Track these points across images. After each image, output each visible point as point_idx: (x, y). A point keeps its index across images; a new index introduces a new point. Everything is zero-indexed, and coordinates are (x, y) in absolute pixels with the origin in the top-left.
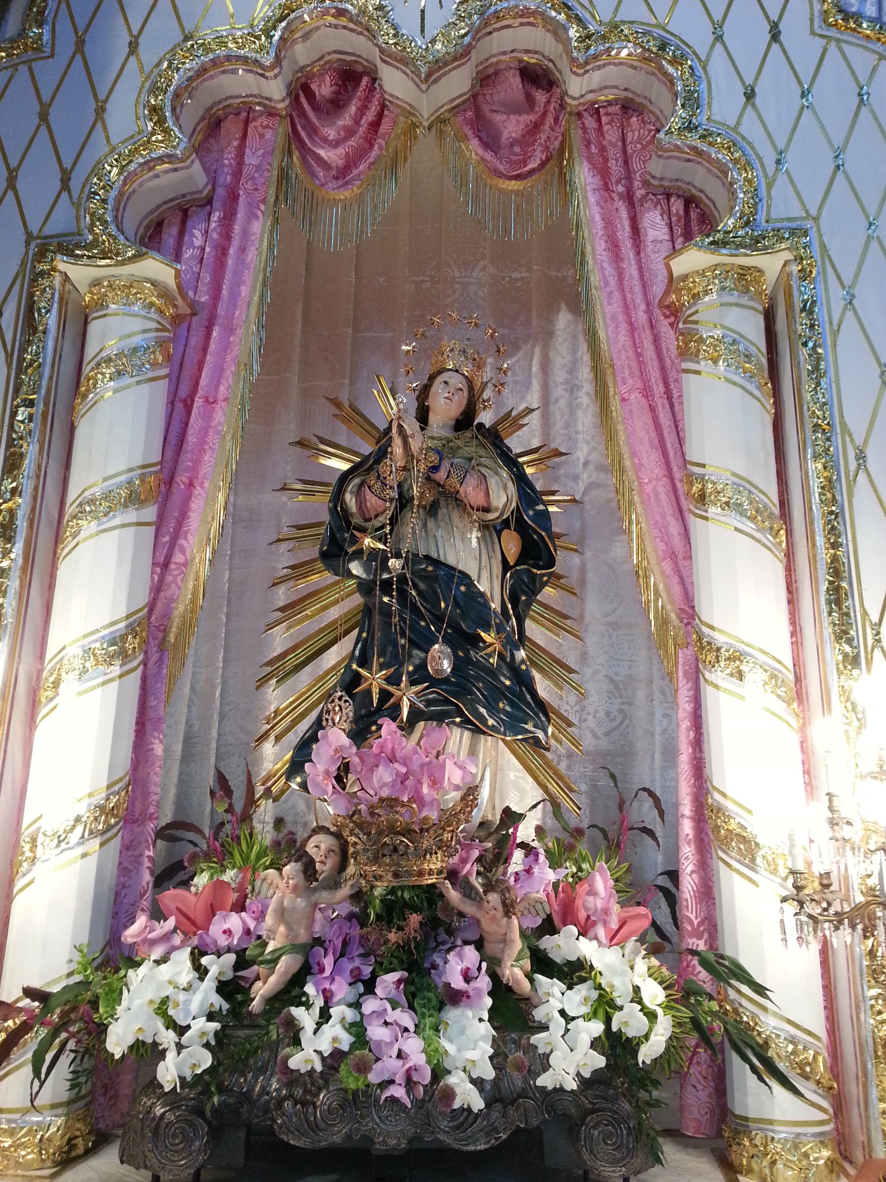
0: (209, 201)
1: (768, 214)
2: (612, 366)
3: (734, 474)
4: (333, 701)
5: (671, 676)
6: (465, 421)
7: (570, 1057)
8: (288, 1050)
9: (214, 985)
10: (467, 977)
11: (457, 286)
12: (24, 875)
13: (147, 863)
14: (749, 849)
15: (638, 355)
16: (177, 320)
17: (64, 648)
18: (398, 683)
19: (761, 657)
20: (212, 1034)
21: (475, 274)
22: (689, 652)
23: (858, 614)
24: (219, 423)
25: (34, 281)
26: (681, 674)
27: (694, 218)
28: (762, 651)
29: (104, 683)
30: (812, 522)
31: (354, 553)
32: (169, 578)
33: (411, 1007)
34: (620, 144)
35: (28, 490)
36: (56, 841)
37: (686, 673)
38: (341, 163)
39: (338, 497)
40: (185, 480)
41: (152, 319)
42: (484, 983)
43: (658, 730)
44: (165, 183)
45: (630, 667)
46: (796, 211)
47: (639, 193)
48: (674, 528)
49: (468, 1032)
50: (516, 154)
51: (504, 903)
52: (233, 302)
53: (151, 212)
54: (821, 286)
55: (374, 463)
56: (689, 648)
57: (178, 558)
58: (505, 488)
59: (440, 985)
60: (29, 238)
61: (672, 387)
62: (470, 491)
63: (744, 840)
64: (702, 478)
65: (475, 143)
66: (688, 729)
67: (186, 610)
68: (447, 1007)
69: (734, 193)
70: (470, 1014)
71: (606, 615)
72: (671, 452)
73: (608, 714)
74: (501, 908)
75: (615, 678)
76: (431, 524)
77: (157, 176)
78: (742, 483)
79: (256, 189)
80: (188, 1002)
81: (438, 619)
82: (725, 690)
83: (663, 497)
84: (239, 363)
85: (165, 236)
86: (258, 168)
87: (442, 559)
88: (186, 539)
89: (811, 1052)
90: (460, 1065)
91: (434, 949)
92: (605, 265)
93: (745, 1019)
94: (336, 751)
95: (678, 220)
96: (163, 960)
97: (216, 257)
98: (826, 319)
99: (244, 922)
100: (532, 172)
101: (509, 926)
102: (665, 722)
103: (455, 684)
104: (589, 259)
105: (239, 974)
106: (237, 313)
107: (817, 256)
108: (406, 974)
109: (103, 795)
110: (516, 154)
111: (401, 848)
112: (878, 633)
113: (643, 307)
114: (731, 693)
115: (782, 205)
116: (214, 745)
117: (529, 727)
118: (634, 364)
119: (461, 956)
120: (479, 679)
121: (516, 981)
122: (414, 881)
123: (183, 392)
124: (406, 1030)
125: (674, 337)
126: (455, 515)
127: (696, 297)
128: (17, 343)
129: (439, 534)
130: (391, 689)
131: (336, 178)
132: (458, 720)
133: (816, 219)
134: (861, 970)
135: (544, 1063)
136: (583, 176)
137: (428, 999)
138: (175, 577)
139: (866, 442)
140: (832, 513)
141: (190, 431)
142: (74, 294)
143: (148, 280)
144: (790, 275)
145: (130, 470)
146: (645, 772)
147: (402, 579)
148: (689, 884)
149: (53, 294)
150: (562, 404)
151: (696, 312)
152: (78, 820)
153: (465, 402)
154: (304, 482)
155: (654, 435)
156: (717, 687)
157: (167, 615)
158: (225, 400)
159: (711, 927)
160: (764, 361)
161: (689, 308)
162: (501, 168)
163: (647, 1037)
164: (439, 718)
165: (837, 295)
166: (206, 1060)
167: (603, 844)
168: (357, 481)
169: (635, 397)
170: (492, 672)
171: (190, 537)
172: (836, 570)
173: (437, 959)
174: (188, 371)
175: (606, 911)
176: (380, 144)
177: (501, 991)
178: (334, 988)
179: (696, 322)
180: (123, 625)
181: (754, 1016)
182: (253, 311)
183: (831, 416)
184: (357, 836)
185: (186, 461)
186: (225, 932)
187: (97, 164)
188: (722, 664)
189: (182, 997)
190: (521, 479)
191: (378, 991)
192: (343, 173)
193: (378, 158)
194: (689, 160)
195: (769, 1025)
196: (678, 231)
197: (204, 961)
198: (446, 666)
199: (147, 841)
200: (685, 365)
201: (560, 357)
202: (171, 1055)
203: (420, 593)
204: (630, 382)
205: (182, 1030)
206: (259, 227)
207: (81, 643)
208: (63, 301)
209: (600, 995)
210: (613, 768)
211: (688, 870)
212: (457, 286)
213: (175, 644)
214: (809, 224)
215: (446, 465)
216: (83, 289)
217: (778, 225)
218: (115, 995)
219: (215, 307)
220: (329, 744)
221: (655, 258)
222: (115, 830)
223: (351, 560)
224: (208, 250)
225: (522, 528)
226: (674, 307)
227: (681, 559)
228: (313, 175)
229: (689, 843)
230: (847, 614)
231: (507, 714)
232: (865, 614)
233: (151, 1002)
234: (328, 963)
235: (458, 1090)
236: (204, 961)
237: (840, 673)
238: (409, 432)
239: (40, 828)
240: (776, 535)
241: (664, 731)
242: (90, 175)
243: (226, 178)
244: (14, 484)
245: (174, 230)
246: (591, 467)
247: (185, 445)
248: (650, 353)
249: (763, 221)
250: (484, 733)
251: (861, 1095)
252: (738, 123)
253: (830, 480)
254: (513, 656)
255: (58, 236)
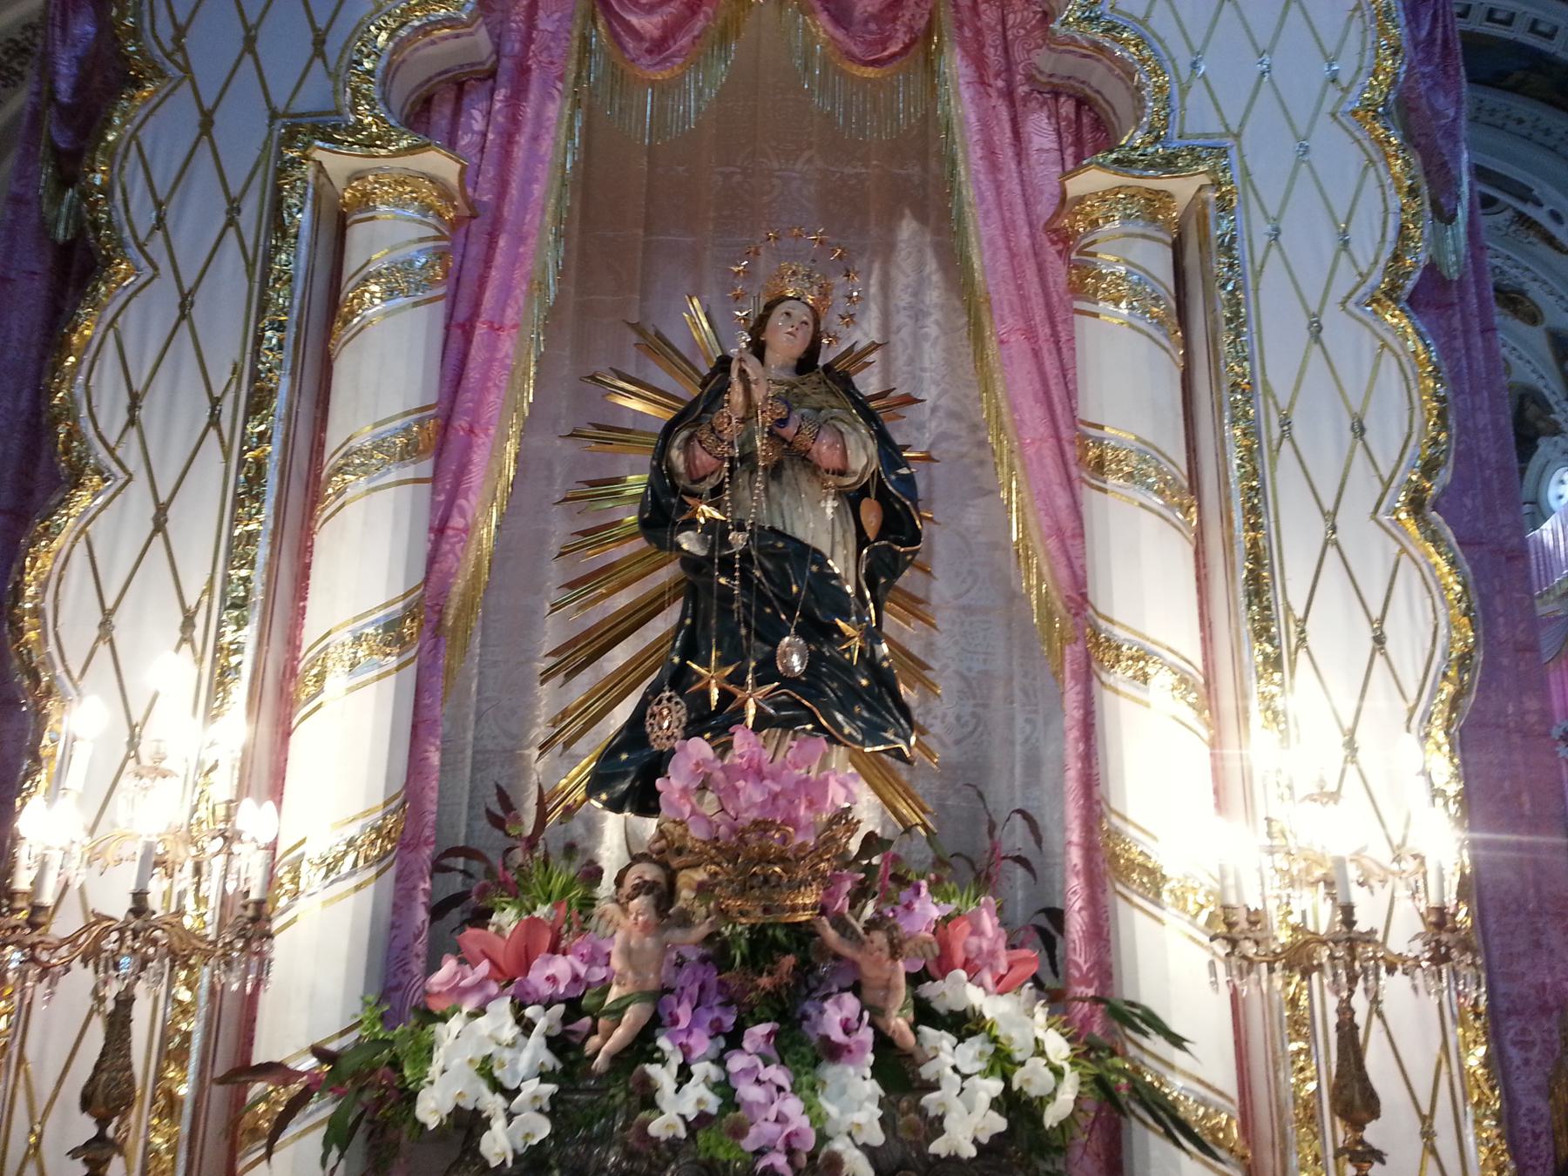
0: (492, 74)
1: (1182, 128)
2: (988, 301)
3: (1138, 439)
4: (660, 702)
5: (1057, 675)
6: (806, 363)
7: (967, 1119)
8: (643, 1115)
9: (543, 1041)
10: (847, 1030)
11: (776, 181)
12: (282, 913)
13: (422, 898)
14: (1154, 880)
15: (1019, 287)
16: (454, 225)
17: (329, 633)
18: (742, 683)
19: (1170, 657)
20: (546, 1099)
21: (798, 166)
22: (1079, 648)
23: (1281, 609)
24: (507, 356)
25: (281, 172)
26: (1068, 674)
27: (1090, 128)
28: (1169, 650)
29: (379, 677)
30: (1228, 499)
31: (684, 522)
32: (446, 547)
33: (782, 1063)
34: (999, 28)
35: (278, 438)
36: (324, 870)
37: (1074, 672)
38: (657, 33)
39: (662, 453)
40: (464, 424)
41: (428, 224)
42: (866, 1035)
43: (1019, 738)
44: (445, 51)
45: (985, 661)
46: (1214, 126)
47: (1022, 90)
48: (1062, 500)
49: (851, 1091)
50: (871, 33)
51: (891, 942)
52: (524, 205)
53: (421, 86)
54: (1240, 216)
55: (705, 410)
56: (1083, 644)
57: (457, 522)
58: (865, 448)
59: (815, 1040)
60: (274, 115)
61: (1060, 328)
62: (824, 451)
63: (1151, 872)
64: (1099, 442)
65: (823, 19)
66: (1077, 740)
67: (467, 586)
68: (824, 1063)
69: (1141, 100)
70: (851, 1070)
71: (958, 597)
72: (1059, 409)
73: (958, 718)
74: (887, 949)
75: (966, 673)
76: (773, 489)
77: (433, 43)
78: (1148, 452)
79: (552, 63)
80: (515, 1061)
81: (790, 606)
82: (1127, 696)
83: (1049, 461)
84: (532, 281)
85: (435, 117)
86: (554, 35)
87: (789, 532)
88: (466, 499)
89: (1224, 1116)
90: (844, 1128)
91: (808, 996)
92: (982, 177)
93: (1149, 1079)
94: (697, 765)
95: (1069, 126)
96: (480, 1011)
97: (502, 147)
98: (1248, 257)
99: (572, 966)
100: (893, 56)
101: (894, 971)
102: (1028, 729)
103: (807, 684)
104: (961, 169)
105: (570, 1027)
106: (528, 217)
107: (1238, 181)
108: (777, 1026)
109: (379, 814)
110: (871, 33)
111: (774, 880)
112: (1303, 631)
113: (1026, 230)
114: (1134, 699)
115: (1198, 119)
116: (469, 752)
117: (890, 735)
118: (1015, 299)
119: (839, 1005)
120: (833, 677)
121: (902, 1034)
122: (788, 917)
123: (462, 313)
124: (780, 1089)
125: (1064, 270)
126: (803, 478)
127: (1094, 224)
128: (261, 249)
129: (785, 500)
130: (731, 687)
131: (650, 52)
132: (809, 727)
133: (1237, 136)
134: (1281, 1021)
135: (936, 1126)
136: (954, 65)
137: (806, 1054)
138: (453, 545)
139: (1291, 405)
140: (1252, 488)
141: (471, 364)
142: (328, 187)
143: (425, 175)
144: (1205, 203)
145: (407, 414)
146: (1004, 794)
147: (746, 555)
148: (1076, 923)
149: (306, 189)
150: (905, 333)
151: (1093, 242)
152: (351, 843)
153: (809, 338)
154: (599, 427)
155: (1038, 386)
156: (1116, 691)
157: (443, 593)
158: (515, 326)
159: (1104, 971)
160: (1173, 304)
161: (1085, 237)
162: (856, 50)
163: (1052, 1096)
164: (787, 724)
165: (1261, 229)
166: (543, 1128)
167: (971, 876)
168: (684, 434)
169: (1017, 339)
170: (847, 668)
171: (471, 497)
172: (1256, 556)
173: (809, 1008)
174: (467, 290)
175: (993, 954)
176: (706, 13)
177: (884, 1043)
178: (692, 1041)
179: (1094, 254)
180: (400, 605)
181: (1159, 1077)
182: (548, 218)
183: (1252, 373)
184: (719, 864)
185: (466, 399)
186: (548, 978)
187: (360, 24)
188: (1123, 664)
189: (507, 1055)
190: (883, 438)
191: (746, 1044)
192: (659, 46)
193: (705, 30)
194: (1085, 56)
195: (1175, 1086)
196: (1068, 138)
197: (529, 1012)
198: (796, 663)
199: (421, 870)
200: (1077, 305)
201: (903, 279)
202: (498, 1125)
203: (765, 571)
204: (1010, 321)
205: (510, 1094)
206: (556, 109)
207: (350, 628)
208: (317, 198)
209: (997, 1050)
210: (970, 781)
211: (1077, 906)
212: (776, 181)
213: (454, 628)
214: (1229, 142)
215: (795, 416)
216: (339, 184)
217: (1193, 142)
218: (424, 1054)
219: (499, 208)
220: (688, 756)
221: (1045, 171)
222: (391, 857)
223: (680, 531)
224: (491, 136)
225: (883, 496)
226: (1064, 234)
227: (1071, 536)
228: (623, 48)
229: (1077, 874)
230: (1268, 608)
231: (864, 720)
232: (1288, 608)
233: (471, 1061)
234: (684, 1013)
235: (846, 1158)
236: (529, 1012)
237: (1259, 677)
238: (752, 377)
239: (303, 854)
240: (1186, 513)
241: (1027, 740)
242: (350, 39)
243: (513, 45)
244: (262, 428)
245: (447, 110)
246: (941, 414)
247: (464, 382)
248: (1034, 288)
249: (1175, 135)
250: (839, 743)
251: (1278, 1166)
252: (1147, 16)
253: (1249, 449)
254: (873, 651)
255: (309, 114)
